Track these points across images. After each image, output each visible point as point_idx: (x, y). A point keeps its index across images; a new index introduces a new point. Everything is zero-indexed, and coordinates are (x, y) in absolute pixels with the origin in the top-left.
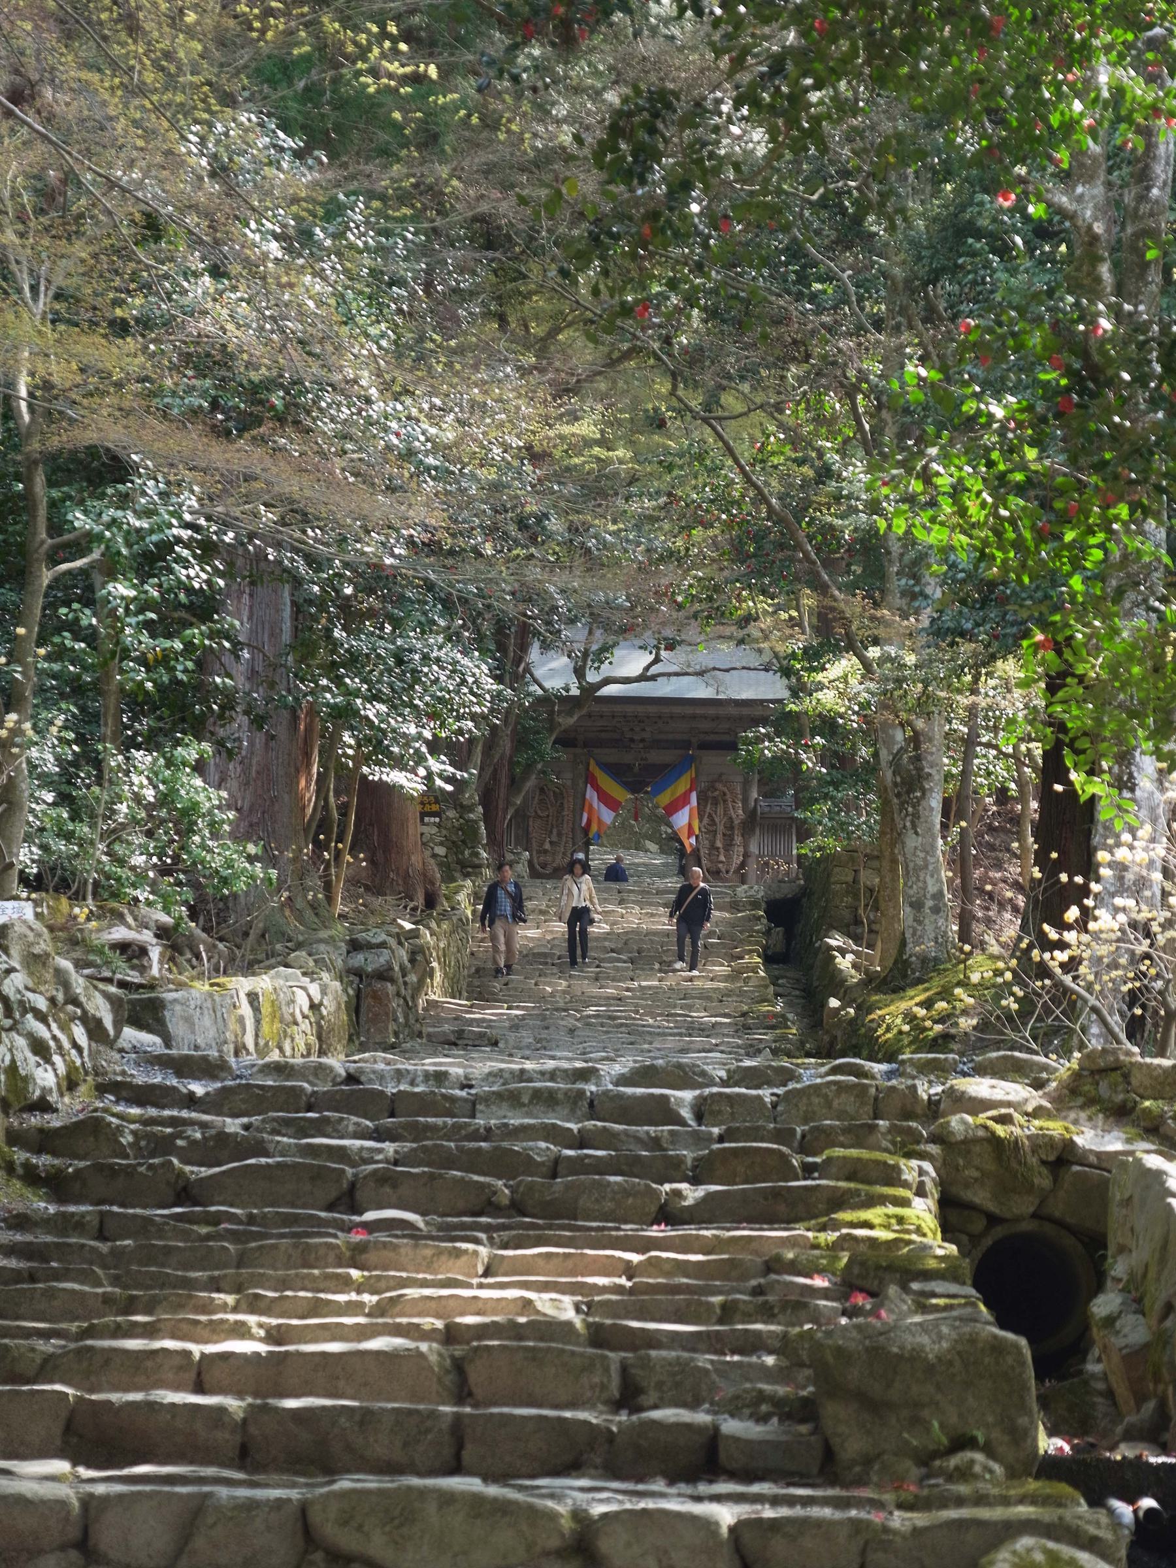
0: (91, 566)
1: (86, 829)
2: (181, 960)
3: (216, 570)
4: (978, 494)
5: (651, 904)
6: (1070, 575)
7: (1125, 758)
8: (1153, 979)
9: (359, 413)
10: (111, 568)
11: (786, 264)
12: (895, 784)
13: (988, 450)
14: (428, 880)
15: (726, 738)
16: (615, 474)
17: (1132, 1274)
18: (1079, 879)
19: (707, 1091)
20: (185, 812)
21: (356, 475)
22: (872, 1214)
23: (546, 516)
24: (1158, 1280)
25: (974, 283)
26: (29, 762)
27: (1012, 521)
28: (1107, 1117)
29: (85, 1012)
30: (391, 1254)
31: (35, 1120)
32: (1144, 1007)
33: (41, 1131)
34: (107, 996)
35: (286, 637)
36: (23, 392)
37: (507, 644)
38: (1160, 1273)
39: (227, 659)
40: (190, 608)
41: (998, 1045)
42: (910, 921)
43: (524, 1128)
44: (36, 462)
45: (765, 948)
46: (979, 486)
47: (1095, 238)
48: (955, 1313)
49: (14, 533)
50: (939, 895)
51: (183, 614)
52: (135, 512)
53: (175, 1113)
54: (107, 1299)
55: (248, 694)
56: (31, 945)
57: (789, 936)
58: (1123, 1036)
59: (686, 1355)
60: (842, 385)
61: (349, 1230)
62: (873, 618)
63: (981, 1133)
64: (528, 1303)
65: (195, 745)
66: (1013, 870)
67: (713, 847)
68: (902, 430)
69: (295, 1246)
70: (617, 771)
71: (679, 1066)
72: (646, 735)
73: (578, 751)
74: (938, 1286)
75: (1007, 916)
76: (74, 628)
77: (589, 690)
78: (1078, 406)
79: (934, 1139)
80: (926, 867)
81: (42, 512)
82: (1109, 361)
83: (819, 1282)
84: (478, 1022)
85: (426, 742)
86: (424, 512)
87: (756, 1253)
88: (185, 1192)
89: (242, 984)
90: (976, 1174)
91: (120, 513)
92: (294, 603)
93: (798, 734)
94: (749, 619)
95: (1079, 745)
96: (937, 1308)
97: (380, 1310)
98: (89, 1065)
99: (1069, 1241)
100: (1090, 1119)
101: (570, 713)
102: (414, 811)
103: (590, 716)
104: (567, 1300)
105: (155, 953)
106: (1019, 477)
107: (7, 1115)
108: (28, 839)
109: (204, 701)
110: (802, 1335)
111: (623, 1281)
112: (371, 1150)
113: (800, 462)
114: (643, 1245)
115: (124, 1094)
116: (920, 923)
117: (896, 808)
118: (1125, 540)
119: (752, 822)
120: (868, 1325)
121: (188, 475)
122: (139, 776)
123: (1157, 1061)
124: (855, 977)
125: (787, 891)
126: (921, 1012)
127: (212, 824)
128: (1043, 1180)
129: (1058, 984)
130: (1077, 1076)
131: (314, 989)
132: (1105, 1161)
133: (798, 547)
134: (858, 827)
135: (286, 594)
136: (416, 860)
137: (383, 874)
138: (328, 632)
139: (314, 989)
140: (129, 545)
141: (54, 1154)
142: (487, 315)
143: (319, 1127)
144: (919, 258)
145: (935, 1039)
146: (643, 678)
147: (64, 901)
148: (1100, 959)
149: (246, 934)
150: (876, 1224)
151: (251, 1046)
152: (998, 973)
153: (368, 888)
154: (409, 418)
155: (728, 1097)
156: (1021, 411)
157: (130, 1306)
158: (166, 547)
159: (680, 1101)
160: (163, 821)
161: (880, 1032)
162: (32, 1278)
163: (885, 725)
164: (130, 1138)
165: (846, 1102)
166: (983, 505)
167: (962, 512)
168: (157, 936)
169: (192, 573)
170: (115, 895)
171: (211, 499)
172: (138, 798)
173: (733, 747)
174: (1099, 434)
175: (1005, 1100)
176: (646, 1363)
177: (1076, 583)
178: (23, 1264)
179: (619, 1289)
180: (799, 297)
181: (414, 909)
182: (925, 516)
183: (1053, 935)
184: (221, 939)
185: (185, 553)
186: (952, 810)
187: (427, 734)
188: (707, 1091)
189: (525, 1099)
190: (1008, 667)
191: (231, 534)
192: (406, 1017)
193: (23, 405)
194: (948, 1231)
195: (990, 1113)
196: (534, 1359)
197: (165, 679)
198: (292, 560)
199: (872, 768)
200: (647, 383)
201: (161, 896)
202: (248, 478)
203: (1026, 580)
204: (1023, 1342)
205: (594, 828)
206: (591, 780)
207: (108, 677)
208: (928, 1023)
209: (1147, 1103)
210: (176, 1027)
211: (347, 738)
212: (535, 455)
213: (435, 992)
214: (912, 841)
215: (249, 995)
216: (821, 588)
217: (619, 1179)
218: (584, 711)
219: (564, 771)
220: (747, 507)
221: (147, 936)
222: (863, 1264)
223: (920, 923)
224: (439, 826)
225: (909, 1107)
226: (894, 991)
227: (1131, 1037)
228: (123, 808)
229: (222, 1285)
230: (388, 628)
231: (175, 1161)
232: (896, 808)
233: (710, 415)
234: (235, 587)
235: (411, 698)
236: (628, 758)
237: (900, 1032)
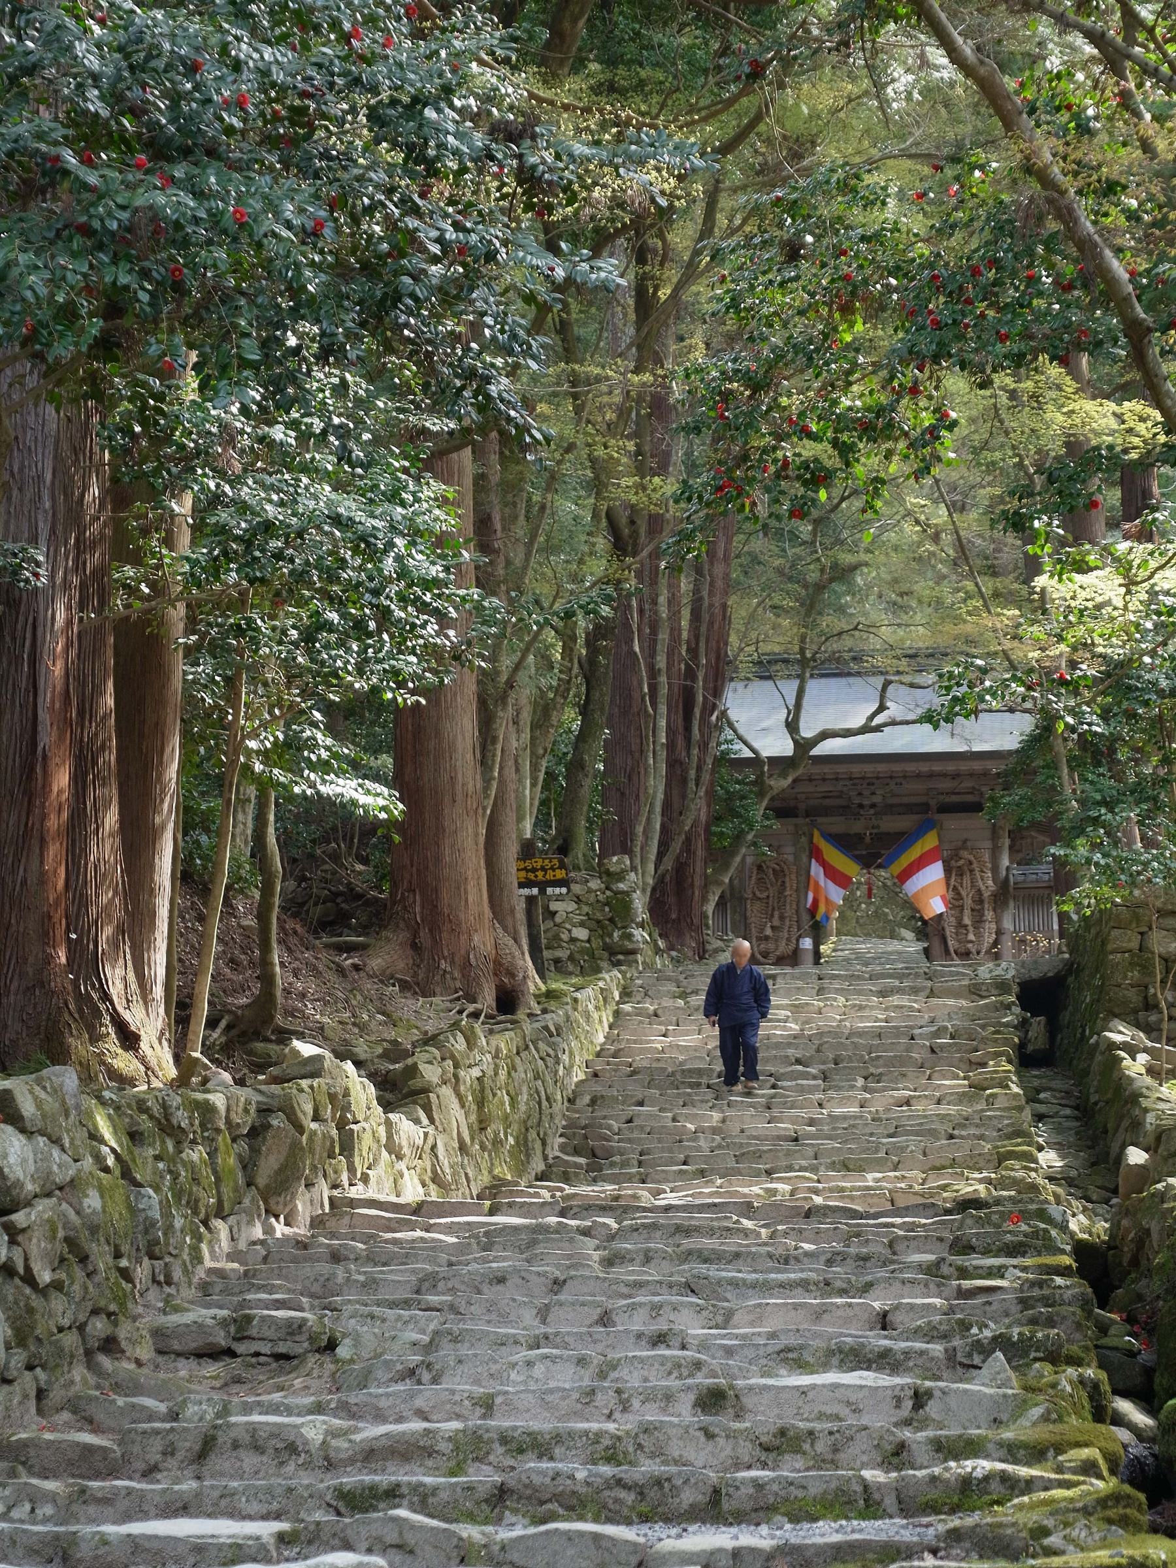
5: (859, 993)
57: (1053, 1028)
67: (960, 925)
72: (877, 799)
73: (800, 821)
77: (803, 746)
101: (784, 775)
119: (1004, 894)
146: (865, 729)
153: (405, 986)
205: (822, 909)
236: (857, 827)
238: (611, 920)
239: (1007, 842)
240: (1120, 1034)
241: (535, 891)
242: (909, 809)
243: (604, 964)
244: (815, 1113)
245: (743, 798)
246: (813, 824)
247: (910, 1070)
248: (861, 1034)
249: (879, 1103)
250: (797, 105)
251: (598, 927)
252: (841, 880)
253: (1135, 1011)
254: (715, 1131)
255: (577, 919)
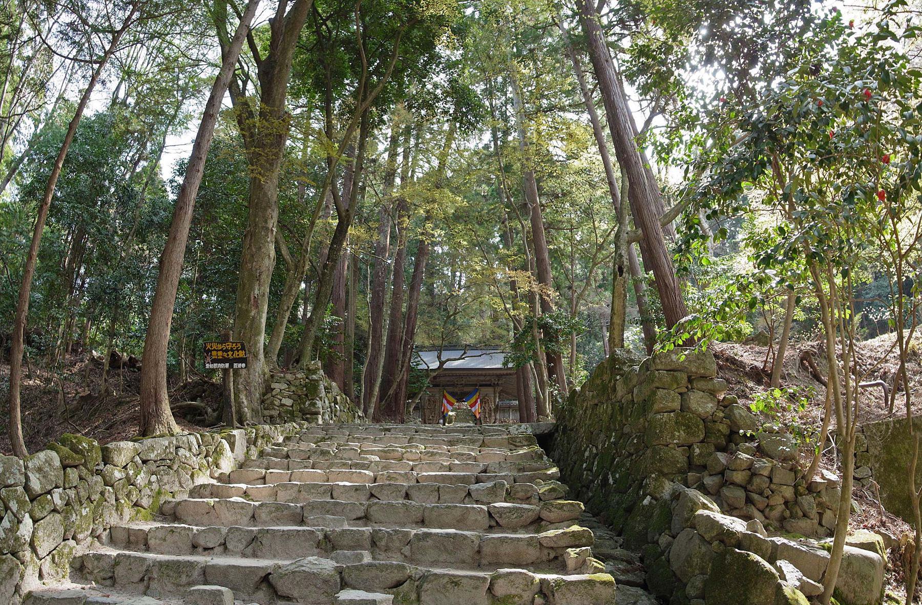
30: (622, 578)
70: (453, 395)
236: (456, 390)
238: (306, 395)
241: (227, 365)
242: (472, 385)
250: (585, 450)
251: (298, 398)
255: (286, 393)
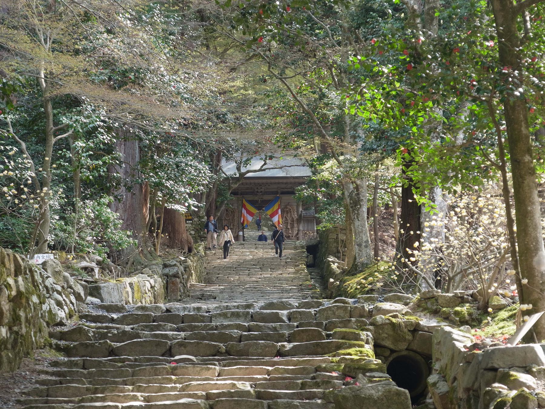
0: (69, 136)
1: (71, 228)
2: (105, 272)
3: (113, 137)
4: (380, 99)
5: (266, 248)
6: (412, 127)
7: (432, 191)
8: (444, 267)
9: (160, 80)
10: (76, 136)
11: (306, 24)
12: (351, 203)
13: (383, 84)
14: (189, 242)
15: (290, 190)
16: (248, 99)
17: (441, 368)
18: (418, 232)
19: (292, 310)
20: (105, 221)
21: (160, 101)
22: (352, 351)
23: (226, 114)
24: (451, 369)
25: (373, 28)
26: (50, 205)
27: (392, 109)
28: (430, 314)
29: (74, 291)
30: (186, 370)
31: (58, 329)
32: (440, 276)
33: (61, 332)
34: (81, 285)
35: (137, 159)
36: (43, 76)
37: (214, 159)
38: (451, 367)
39: (117, 167)
40: (104, 150)
41: (390, 292)
42: (357, 251)
43: (229, 326)
44: (48, 101)
45: (307, 262)
46: (380, 97)
47: (415, 10)
48: (383, 383)
49: (41, 126)
50: (367, 241)
51: (101, 152)
52: (84, 117)
53: (107, 325)
54: (88, 389)
55: (125, 179)
56: (54, 268)
57: (315, 258)
58: (434, 287)
59: (290, 400)
60: (327, 65)
61: (170, 363)
62: (342, 146)
63: (387, 321)
64: (234, 385)
65: (108, 197)
66: (392, 232)
67: (287, 228)
68: (348, 79)
69: (152, 369)
71: (282, 302)
72: (262, 190)
73: (239, 196)
74: (376, 374)
75: (390, 248)
76: (63, 157)
77: (242, 175)
78: (414, 67)
79: (371, 324)
80: (362, 232)
81: (51, 118)
82: (424, 52)
83: (334, 374)
84: (209, 291)
85: (187, 194)
86: (185, 112)
87: (311, 365)
88: (112, 352)
89: (127, 280)
90: (386, 336)
91: (78, 117)
92: (140, 147)
93: (315, 188)
94: (298, 147)
95: (417, 185)
96: (376, 381)
97: (183, 389)
98: (76, 309)
99: (419, 358)
100: (425, 315)
101: (236, 183)
102: (183, 219)
103: (242, 184)
104: (248, 384)
105: (97, 270)
106: (394, 93)
107: (49, 327)
108: (50, 232)
109: (110, 182)
110: (330, 392)
111: (266, 376)
112: (176, 335)
113: (314, 93)
114: (273, 364)
115: (89, 319)
116: (361, 251)
117: (351, 211)
118: (431, 114)
119: (300, 219)
120: (353, 387)
121: (102, 104)
122: (88, 209)
123: (447, 294)
124: (338, 271)
125: (313, 242)
126: (364, 281)
127: (115, 225)
128: (409, 337)
129: (411, 270)
130: (420, 300)
131: (152, 281)
132: (430, 330)
133: (314, 122)
134: (338, 219)
135: (137, 144)
136: (184, 236)
137: (174, 241)
138: (152, 157)
139: (152, 281)
140: (82, 129)
141: (66, 340)
142: (202, 44)
143: (158, 328)
144: (353, 20)
145: (368, 291)
147: (64, 253)
148: (425, 261)
149: (127, 263)
150: (353, 354)
151: (131, 302)
152: (390, 267)
153: (168, 246)
154: (177, 82)
155: (299, 312)
156: (394, 70)
157: (96, 391)
158: (95, 129)
159: (282, 314)
160: (97, 224)
161: (349, 289)
162: (61, 383)
163: (346, 182)
164: (92, 334)
165: (340, 312)
166: (382, 103)
167: (374, 106)
168: (97, 264)
169: (105, 137)
170: (82, 251)
171: (110, 111)
172: (88, 216)
173: (293, 193)
174: (422, 77)
175: (395, 310)
176: (276, 404)
177: (414, 129)
178: (58, 378)
179: (265, 379)
180: (312, 35)
181: (184, 253)
182: (362, 107)
183: (410, 252)
184: (119, 265)
185: (102, 130)
186: (371, 212)
187: (188, 191)
188: (292, 310)
189: (229, 315)
190: (388, 161)
191: (117, 124)
192: (184, 290)
193: (43, 80)
194: (377, 356)
195: (390, 315)
196: (238, 404)
197: (97, 175)
198: (139, 132)
199: (342, 198)
200: (260, 67)
201: (98, 251)
202: (123, 103)
203: (397, 129)
204: (407, 391)
205: (245, 223)
206: (244, 206)
207: (76, 174)
208: (366, 285)
209: (444, 309)
210: (105, 295)
211: (159, 194)
212: (223, 93)
213: (193, 281)
214: (357, 223)
215: (129, 284)
216: (323, 136)
217: (263, 342)
218: (240, 183)
219: (238, 201)
220: (296, 109)
221: (94, 265)
222: (349, 367)
223: (361, 251)
224: (192, 224)
225: (362, 314)
226: (353, 275)
227: (436, 287)
228: (83, 220)
229: (127, 383)
230: (172, 155)
231: (108, 341)
232: (351, 211)
233: (282, 77)
234: (119, 142)
235: (182, 179)
236: (256, 198)
237: (356, 289)
239: (301, 203)
240: (331, 259)
243: (199, 241)
244: (260, 276)
245: (225, 190)
246: (243, 197)
247: (281, 267)
248: (268, 258)
249: (275, 274)
252: (251, 214)
253: (335, 253)
254: (238, 280)
255: (192, 229)
